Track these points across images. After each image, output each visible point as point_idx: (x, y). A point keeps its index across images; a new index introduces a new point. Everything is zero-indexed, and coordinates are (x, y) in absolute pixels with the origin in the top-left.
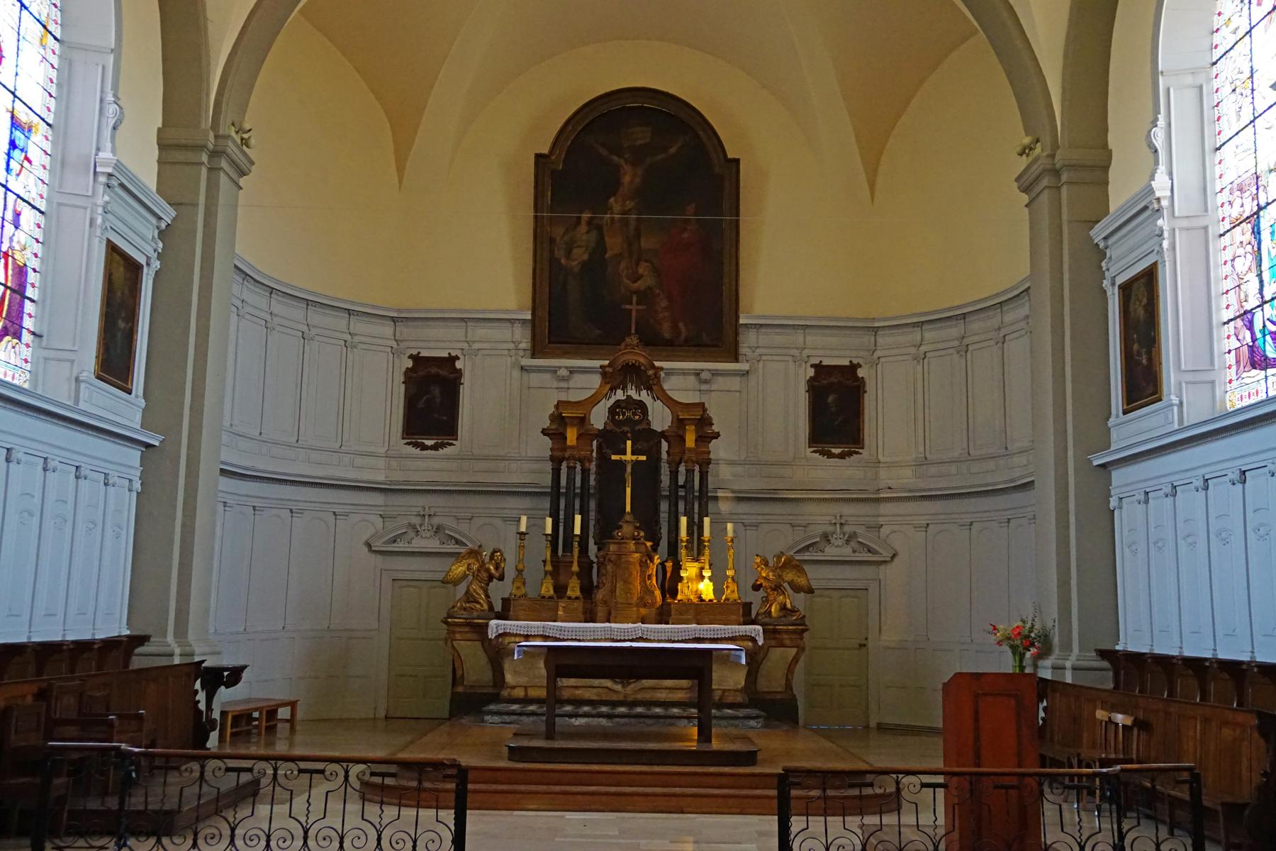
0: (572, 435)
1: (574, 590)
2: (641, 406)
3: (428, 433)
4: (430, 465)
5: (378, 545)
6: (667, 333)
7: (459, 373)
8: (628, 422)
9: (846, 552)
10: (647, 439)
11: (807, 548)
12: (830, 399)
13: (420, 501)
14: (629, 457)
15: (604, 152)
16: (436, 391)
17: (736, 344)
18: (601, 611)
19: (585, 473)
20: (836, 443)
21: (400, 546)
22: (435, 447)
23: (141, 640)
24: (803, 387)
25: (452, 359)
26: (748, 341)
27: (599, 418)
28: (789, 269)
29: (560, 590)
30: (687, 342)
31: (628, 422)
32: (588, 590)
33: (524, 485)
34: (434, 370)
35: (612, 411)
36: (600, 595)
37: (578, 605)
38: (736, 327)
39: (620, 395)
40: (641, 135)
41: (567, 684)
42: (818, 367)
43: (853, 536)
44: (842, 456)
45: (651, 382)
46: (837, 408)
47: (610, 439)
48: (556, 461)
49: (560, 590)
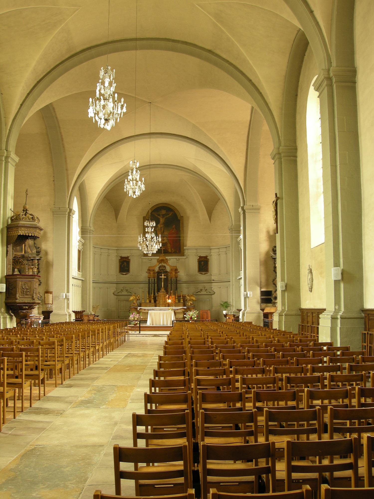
0: (152, 273)
1: (153, 301)
2: (165, 267)
3: (124, 272)
4: (125, 277)
5: (116, 294)
6: (170, 251)
7: (130, 260)
8: (162, 270)
9: (205, 293)
10: (166, 273)
11: (197, 292)
12: (202, 263)
13: (123, 285)
14: (163, 277)
15: (157, 216)
16: (125, 263)
17: (184, 253)
18: (158, 305)
19: (154, 280)
20: (203, 272)
21: (120, 294)
22: (125, 275)
23: (84, 311)
24: (197, 261)
25: (128, 257)
26: (186, 252)
27: (157, 269)
28: (193, 239)
29: (150, 301)
30: (174, 253)
31: (162, 270)
32: (155, 301)
33: (231, 75)
34: (125, 259)
35: (159, 268)
36: (157, 302)
37: (154, 304)
38: (184, 250)
39: (161, 265)
40: (164, 212)
41: (295, 475)
42: (200, 257)
43: (206, 290)
44: (204, 274)
45: (165, 261)
46: (204, 264)
47: (159, 273)
48: (149, 278)
49: (150, 301)
